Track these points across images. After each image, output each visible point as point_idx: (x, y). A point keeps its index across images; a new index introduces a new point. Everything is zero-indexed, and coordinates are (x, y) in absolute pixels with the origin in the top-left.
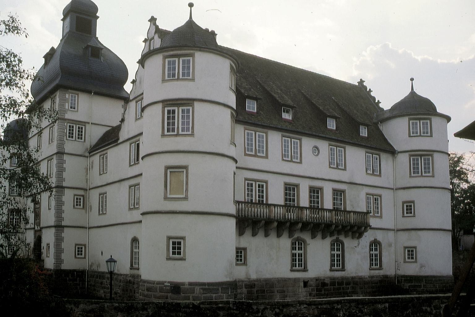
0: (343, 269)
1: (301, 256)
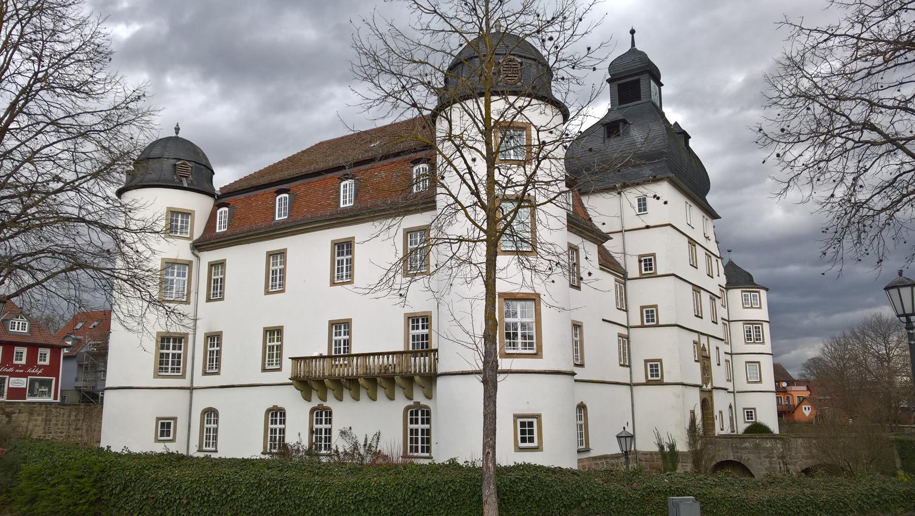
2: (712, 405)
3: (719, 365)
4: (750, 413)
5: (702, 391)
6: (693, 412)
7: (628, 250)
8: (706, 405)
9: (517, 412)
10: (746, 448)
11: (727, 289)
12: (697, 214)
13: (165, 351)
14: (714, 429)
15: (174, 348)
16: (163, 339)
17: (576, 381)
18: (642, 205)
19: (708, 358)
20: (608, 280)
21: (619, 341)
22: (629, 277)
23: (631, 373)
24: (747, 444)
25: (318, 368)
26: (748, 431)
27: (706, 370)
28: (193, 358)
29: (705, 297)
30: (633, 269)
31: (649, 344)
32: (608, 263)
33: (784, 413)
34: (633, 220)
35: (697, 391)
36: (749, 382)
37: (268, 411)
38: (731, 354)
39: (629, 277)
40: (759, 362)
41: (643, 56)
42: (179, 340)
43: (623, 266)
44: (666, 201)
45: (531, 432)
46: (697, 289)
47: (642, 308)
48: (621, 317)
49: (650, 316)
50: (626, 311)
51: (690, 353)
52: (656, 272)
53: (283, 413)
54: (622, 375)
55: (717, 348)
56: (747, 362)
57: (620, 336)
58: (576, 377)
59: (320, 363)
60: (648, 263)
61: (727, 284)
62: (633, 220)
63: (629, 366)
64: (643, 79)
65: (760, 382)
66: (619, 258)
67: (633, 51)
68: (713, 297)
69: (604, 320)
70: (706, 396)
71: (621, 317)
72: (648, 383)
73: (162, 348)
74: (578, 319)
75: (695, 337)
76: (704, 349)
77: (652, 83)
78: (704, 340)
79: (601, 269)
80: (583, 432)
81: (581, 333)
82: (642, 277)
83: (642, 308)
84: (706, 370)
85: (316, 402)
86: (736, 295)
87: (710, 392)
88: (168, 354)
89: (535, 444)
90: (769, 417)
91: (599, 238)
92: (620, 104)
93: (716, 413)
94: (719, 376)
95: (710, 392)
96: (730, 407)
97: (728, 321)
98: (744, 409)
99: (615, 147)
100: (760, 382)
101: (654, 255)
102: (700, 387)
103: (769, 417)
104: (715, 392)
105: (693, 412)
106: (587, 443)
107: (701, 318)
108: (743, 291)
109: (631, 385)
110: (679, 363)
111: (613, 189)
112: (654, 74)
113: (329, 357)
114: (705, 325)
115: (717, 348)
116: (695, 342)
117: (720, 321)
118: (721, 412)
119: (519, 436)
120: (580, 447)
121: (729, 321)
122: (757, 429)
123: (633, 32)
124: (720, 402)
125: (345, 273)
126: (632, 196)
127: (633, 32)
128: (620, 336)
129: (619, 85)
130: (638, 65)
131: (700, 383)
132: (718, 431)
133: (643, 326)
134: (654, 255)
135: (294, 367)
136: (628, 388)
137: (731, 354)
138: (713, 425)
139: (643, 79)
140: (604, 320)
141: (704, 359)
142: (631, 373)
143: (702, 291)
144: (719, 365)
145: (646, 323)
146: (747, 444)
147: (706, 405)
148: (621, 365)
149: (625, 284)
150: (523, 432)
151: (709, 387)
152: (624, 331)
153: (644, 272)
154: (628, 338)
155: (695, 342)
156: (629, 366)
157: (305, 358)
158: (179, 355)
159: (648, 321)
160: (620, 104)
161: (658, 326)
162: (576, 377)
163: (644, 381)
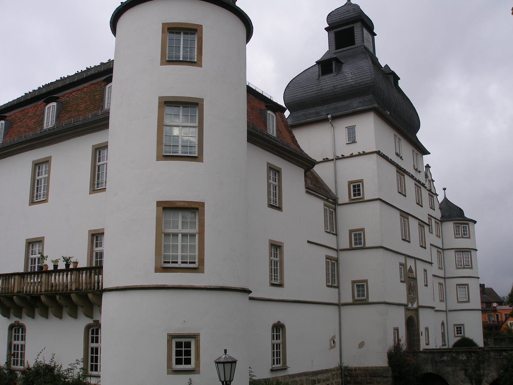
0: (285, 369)
1: (93, 338)
2: (418, 322)
3: (426, 285)
4: (459, 329)
5: (407, 309)
6: (396, 330)
7: (336, 177)
8: (412, 324)
9: (172, 332)
10: (443, 361)
11: (442, 222)
12: (406, 149)
14: (419, 345)
17: (251, 299)
19: (415, 279)
20: (317, 205)
21: (327, 263)
22: (340, 202)
23: (339, 294)
24: (445, 358)
26: (456, 345)
27: (412, 289)
28: (448, 332)
29: (414, 225)
30: (343, 196)
31: (357, 266)
32: (316, 187)
33: (489, 330)
35: (402, 310)
36: (459, 302)
38: (444, 278)
39: (340, 202)
40: (467, 285)
41: (356, 7)
43: (333, 191)
44: (369, 130)
45: (188, 353)
46: (405, 215)
47: (351, 231)
48: (330, 240)
49: (358, 239)
50: (336, 235)
51: (394, 274)
52: (363, 198)
54: (331, 295)
55: (425, 271)
56: (457, 285)
57: (328, 258)
58: (251, 295)
60: (356, 188)
61: (442, 217)
63: (338, 287)
64: (357, 28)
65: (468, 301)
66: (330, 185)
68: (422, 224)
69: (309, 242)
70: (410, 314)
71: (330, 240)
72: (356, 303)
74: (277, 239)
75: (402, 259)
76: (411, 270)
77: (365, 31)
78: (410, 263)
79: (307, 192)
80: (279, 352)
81: (281, 253)
82: (352, 202)
83: (351, 231)
84: (412, 289)
86: (449, 227)
87: (416, 310)
89: (192, 366)
90: (476, 334)
91: (306, 164)
92: (336, 49)
93: (422, 329)
94: (426, 295)
95: (416, 310)
96: (443, 324)
97: (441, 250)
98: (455, 325)
99: (330, 82)
100: (468, 301)
102: (405, 306)
103: (476, 334)
104: (421, 312)
105: (396, 330)
106: (285, 362)
107: (409, 242)
108: (455, 224)
109: (339, 305)
110: (386, 285)
112: (368, 25)
114: (413, 249)
115: (425, 271)
116: (401, 264)
117: (428, 246)
118: (427, 329)
119: (174, 357)
120: (275, 366)
121: (443, 250)
122: (465, 343)
124: (427, 320)
125: (42, 192)
126: (342, 127)
128: (328, 258)
129: (336, 33)
130: (352, 14)
131: (405, 302)
132: (423, 346)
133: (351, 249)
136: (335, 309)
137: (444, 278)
138: (419, 341)
139: (357, 28)
140: (309, 242)
141: (410, 281)
142: (339, 294)
143: (410, 218)
144: (426, 285)
145: (354, 246)
146: (445, 358)
147: (412, 324)
148: (328, 286)
149: (335, 210)
150: (178, 353)
151: (415, 306)
152: (333, 254)
153: (353, 197)
154: (337, 260)
155: (401, 264)
156: (338, 287)
159: (356, 244)
160: (336, 49)
161: (364, 248)
162: (251, 295)
163: (350, 300)
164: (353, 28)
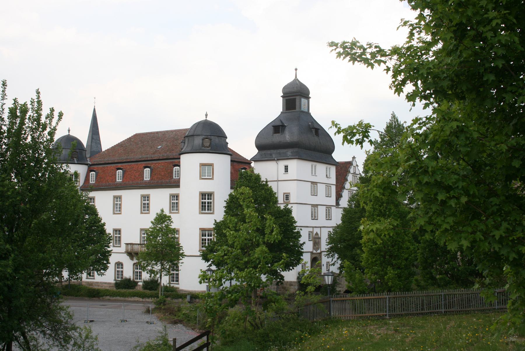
13: (204, 201)
15: (208, 199)
16: (202, 195)
18: (286, 168)
25: (137, 248)
34: (282, 176)
37: (116, 263)
42: (210, 195)
53: (122, 265)
59: (136, 246)
62: (282, 176)
67: (296, 80)
73: (203, 199)
85: (135, 261)
88: (205, 202)
101: (289, 193)
111: (274, 160)
113: (140, 244)
123: (296, 70)
126: (282, 164)
127: (296, 70)
134: (289, 193)
135: (127, 247)
157: (131, 244)
158: (211, 202)
164: (295, 99)
